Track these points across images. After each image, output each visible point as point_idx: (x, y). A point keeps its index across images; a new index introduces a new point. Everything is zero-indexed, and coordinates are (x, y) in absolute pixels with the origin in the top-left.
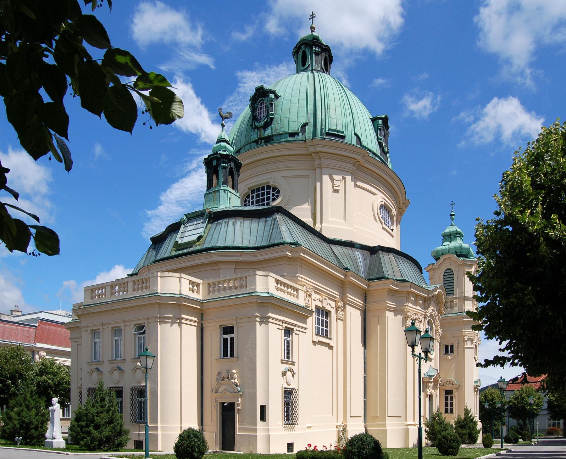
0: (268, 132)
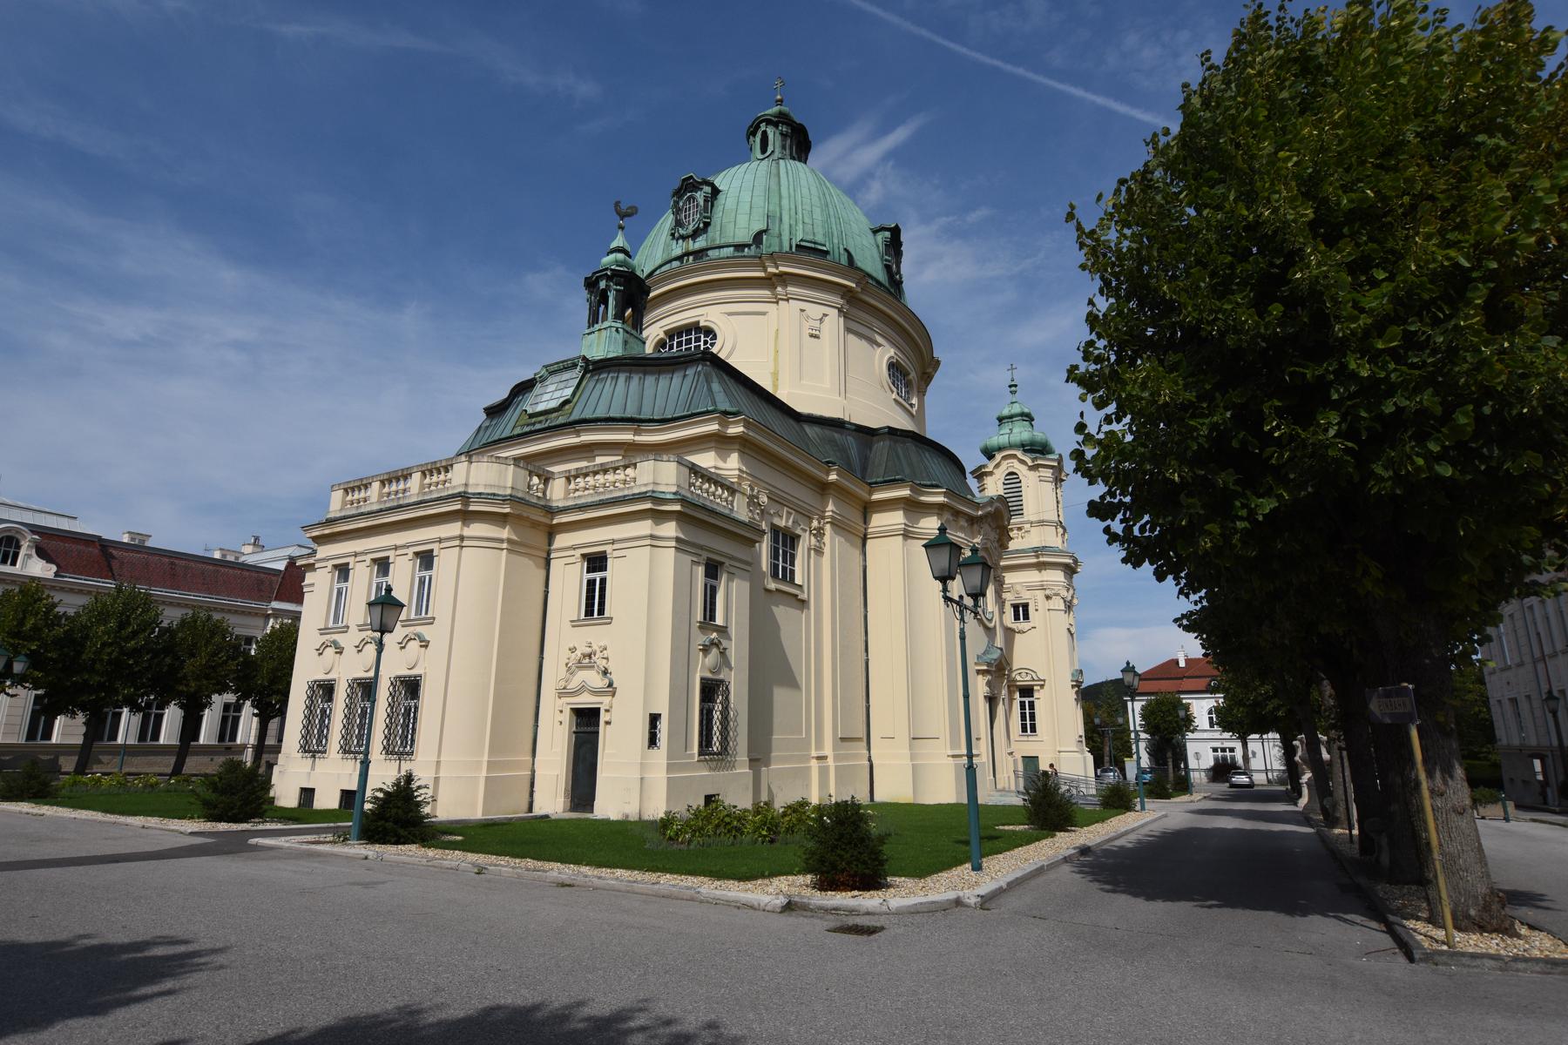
0: (700, 243)
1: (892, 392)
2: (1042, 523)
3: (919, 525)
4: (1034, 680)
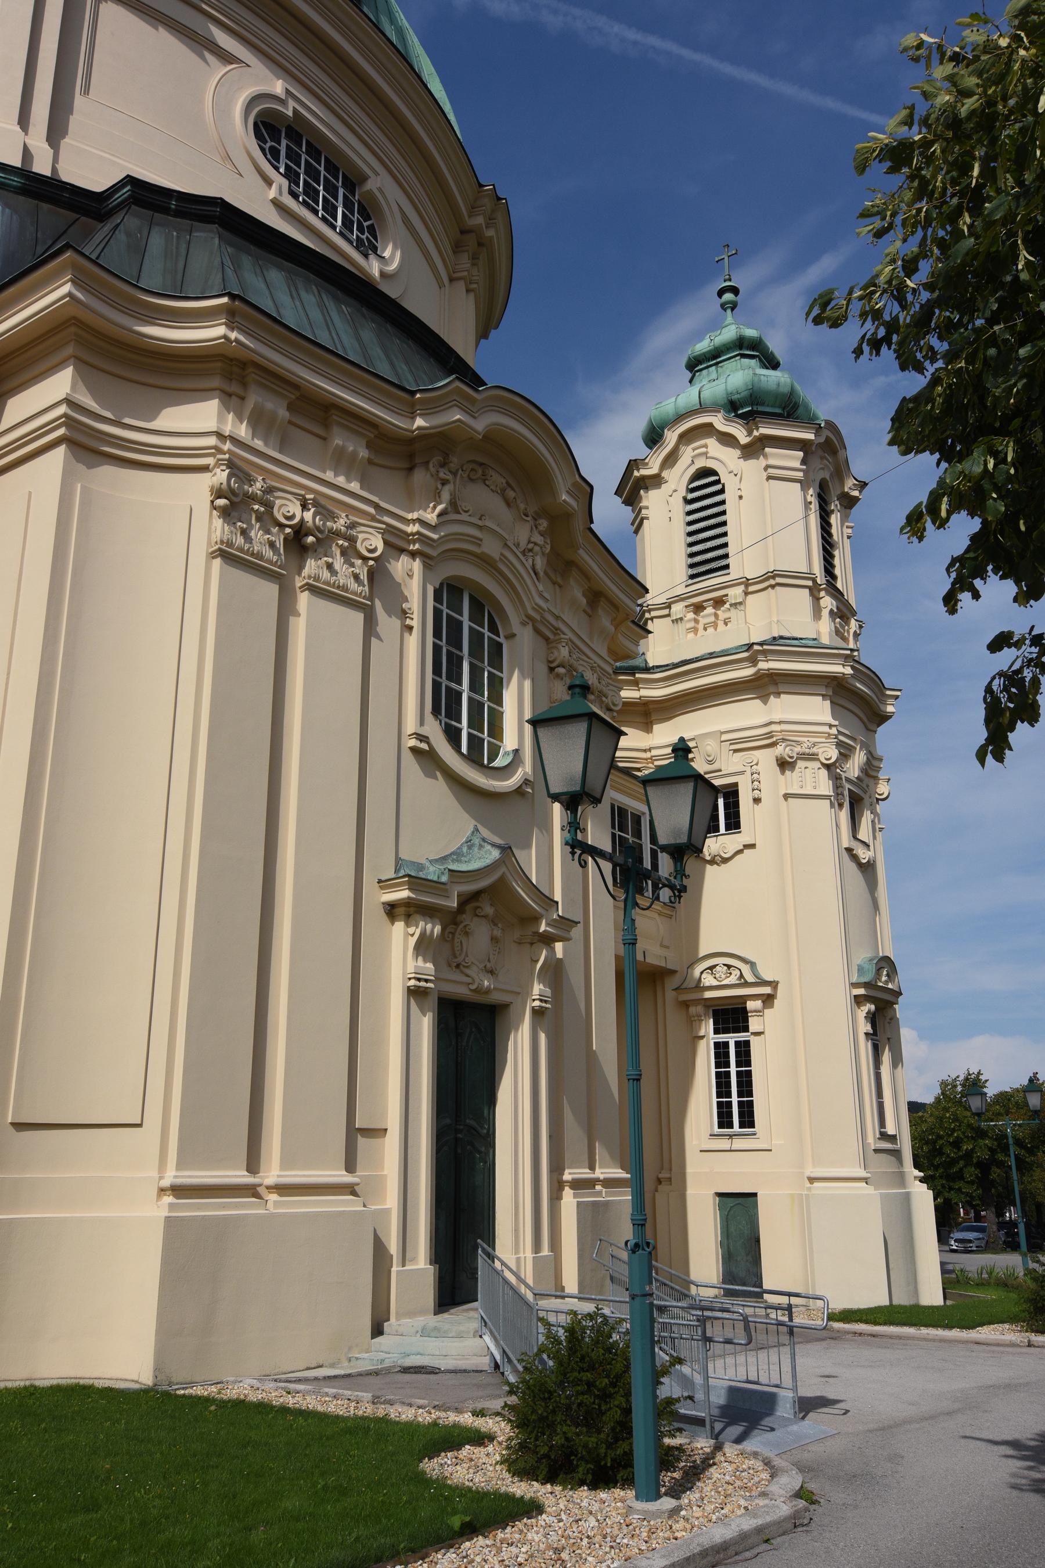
1: (269, 183)
2: (773, 579)
3: (157, 424)
4: (746, 984)
